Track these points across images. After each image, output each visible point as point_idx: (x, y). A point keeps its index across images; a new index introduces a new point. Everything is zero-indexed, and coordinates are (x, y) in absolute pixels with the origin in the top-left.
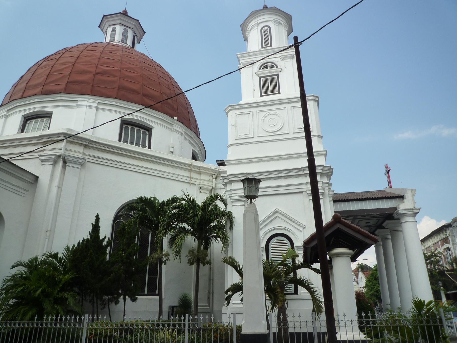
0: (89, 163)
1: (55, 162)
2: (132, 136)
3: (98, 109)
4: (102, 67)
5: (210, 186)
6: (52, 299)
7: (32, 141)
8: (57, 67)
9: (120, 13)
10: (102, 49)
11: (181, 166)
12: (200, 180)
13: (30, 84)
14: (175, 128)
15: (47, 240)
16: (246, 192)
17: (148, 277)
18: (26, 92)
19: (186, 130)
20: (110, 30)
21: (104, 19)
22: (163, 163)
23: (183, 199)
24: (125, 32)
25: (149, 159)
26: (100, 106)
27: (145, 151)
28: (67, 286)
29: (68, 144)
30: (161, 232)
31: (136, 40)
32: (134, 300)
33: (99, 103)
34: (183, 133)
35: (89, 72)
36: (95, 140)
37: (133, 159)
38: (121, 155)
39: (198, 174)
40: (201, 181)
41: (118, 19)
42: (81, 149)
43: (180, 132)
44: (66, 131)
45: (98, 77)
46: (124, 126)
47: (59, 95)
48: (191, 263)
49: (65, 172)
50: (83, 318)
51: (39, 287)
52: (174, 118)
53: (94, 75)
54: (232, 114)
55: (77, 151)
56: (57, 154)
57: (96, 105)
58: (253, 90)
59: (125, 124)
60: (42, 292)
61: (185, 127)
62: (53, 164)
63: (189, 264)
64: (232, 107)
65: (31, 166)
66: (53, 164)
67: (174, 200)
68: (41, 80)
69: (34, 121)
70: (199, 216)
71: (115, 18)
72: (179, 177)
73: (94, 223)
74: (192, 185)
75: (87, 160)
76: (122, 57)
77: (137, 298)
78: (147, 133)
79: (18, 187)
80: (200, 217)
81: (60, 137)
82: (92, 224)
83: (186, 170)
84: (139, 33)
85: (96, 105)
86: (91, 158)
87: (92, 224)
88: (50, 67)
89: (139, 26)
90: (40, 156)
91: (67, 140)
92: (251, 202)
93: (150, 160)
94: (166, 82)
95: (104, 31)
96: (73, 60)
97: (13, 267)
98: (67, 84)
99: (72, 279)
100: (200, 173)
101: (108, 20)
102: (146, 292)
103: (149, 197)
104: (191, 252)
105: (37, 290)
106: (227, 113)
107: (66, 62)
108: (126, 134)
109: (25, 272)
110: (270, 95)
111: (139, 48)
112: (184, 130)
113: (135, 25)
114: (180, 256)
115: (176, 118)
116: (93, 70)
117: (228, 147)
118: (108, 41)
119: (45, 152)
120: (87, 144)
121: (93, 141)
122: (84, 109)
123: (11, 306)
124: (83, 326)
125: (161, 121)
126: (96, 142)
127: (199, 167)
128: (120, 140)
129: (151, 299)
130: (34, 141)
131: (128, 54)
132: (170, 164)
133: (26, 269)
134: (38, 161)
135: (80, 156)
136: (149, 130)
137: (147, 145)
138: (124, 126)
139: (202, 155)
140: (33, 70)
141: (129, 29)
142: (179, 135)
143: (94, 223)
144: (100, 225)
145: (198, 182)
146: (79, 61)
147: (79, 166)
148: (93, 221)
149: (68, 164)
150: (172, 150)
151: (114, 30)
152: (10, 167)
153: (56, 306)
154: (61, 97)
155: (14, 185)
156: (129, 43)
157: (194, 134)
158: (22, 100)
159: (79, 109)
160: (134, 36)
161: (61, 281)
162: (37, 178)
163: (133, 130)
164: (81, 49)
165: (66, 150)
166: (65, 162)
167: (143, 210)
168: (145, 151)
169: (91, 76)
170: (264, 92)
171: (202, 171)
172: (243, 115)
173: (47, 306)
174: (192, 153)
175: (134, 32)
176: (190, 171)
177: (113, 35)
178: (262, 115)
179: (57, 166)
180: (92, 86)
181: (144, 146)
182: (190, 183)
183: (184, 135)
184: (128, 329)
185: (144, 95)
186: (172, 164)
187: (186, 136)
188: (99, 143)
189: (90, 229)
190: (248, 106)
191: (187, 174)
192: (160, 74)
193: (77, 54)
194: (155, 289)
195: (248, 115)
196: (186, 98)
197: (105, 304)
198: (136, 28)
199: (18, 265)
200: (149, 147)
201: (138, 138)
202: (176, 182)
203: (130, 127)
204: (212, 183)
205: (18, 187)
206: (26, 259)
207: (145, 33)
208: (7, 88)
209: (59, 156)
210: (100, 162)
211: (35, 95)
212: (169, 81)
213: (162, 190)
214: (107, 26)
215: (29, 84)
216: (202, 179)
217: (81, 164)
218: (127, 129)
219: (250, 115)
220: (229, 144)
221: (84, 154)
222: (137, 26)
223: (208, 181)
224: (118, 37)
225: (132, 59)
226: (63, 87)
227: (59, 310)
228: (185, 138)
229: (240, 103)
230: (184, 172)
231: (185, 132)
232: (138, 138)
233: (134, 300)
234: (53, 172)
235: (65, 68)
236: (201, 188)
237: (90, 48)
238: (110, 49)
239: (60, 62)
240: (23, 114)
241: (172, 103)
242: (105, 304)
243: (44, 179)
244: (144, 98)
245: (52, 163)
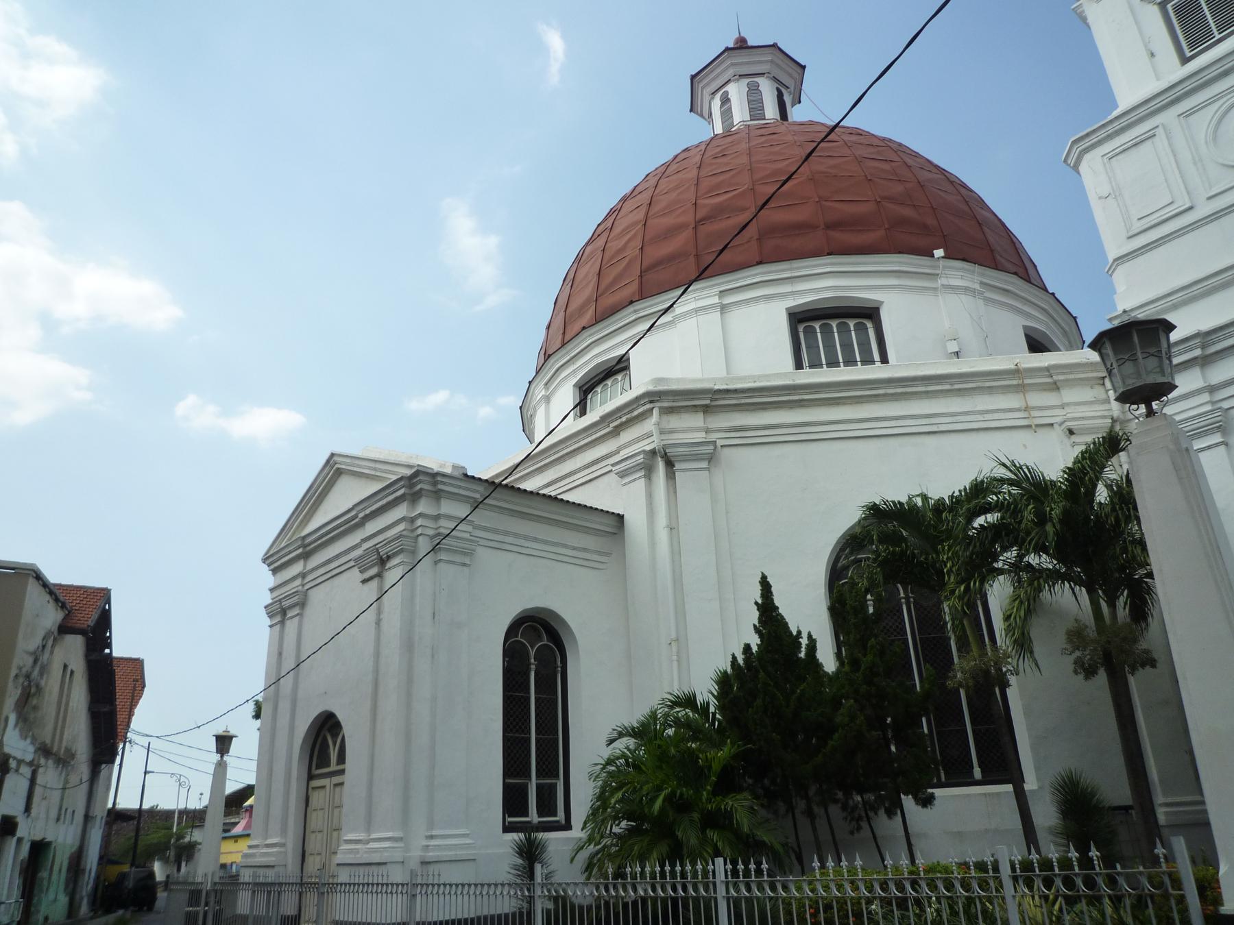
0: (726, 450)
1: (649, 470)
2: (830, 347)
3: (723, 308)
4: (707, 201)
5: (1104, 417)
6: (696, 816)
7: (590, 435)
8: (614, 246)
9: (727, 49)
10: (698, 158)
11: (987, 384)
12: (1063, 406)
13: (572, 308)
14: (944, 281)
15: (675, 664)
16: (1118, 379)
17: (974, 732)
18: (568, 328)
19: (982, 275)
20: (717, 103)
21: (696, 84)
22: (927, 392)
23: (1002, 481)
24: (754, 90)
25: (881, 392)
26: (727, 300)
27: (877, 372)
28: (727, 783)
29: (665, 417)
30: (953, 592)
31: (787, 99)
32: (927, 801)
33: (722, 293)
34: (977, 286)
35: (680, 227)
36: (725, 387)
37: (838, 404)
38: (801, 404)
39: (1051, 390)
40: (1068, 410)
41: (727, 68)
42: (697, 420)
43: (966, 289)
44: (651, 388)
45: (705, 229)
46: (801, 328)
47: (631, 309)
48: (1090, 672)
49: (675, 488)
50: (710, 867)
51: (659, 789)
52: (933, 256)
53: (695, 228)
54: (1093, 169)
55: (689, 429)
56: (648, 448)
57: (716, 300)
58: (1146, 58)
59: (801, 321)
60: (669, 799)
61: (977, 268)
62: (645, 476)
63: (1081, 677)
64: (1085, 144)
65: (603, 495)
66: (645, 476)
67: (979, 489)
68: (588, 291)
69: (599, 389)
70: (1056, 520)
71: (719, 70)
72: (988, 417)
73: (760, 601)
74: (1041, 431)
75: (720, 443)
76: (750, 154)
77: (932, 797)
78: (869, 325)
79: (584, 550)
80: (1060, 521)
81: (643, 405)
82: (756, 603)
83: (1006, 389)
84: (788, 73)
85: (716, 300)
86: (728, 435)
87: (756, 603)
88: (599, 253)
89: (781, 56)
90: (613, 465)
91: (660, 408)
92: (1150, 413)
93: (884, 395)
94: (886, 166)
95: (706, 114)
96: (640, 215)
97: (611, 742)
98: (641, 276)
99: (735, 757)
100: (1055, 387)
101: (705, 81)
102: (977, 773)
103: (904, 500)
104: (1076, 637)
105: (656, 797)
106: (1076, 167)
107: (627, 227)
108: (813, 347)
109: (629, 750)
110: (1219, 41)
111: (797, 114)
112: (977, 278)
113: (772, 61)
114: (1032, 652)
115: (939, 253)
116: (689, 218)
117: (1110, 272)
118: (719, 129)
119: (622, 453)
120: (708, 402)
121: (720, 391)
122: (692, 322)
123: (619, 836)
124: (715, 891)
125: (899, 277)
126: (728, 391)
127: (1047, 369)
128: (799, 365)
129: (998, 794)
130: (595, 433)
131: (763, 139)
132: (948, 387)
133: (631, 742)
134: (613, 477)
135: (700, 436)
136: (870, 313)
137: (876, 356)
138: (801, 328)
139: (1065, 333)
140: (571, 276)
141: (759, 80)
142: (965, 299)
143: (760, 601)
144: (777, 603)
145: (1057, 416)
146: (656, 208)
147: (704, 465)
148: (756, 594)
149: (677, 466)
150: (953, 347)
151: (726, 100)
152: (554, 507)
153: (709, 833)
154: (635, 311)
155: (574, 548)
156: (771, 112)
157: (1014, 279)
158: (563, 351)
159: (682, 326)
160: (778, 90)
161: (710, 767)
162: (620, 517)
163: (826, 330)
164: (653, 182)
165: (662, 433)
166: (669, 464)
167: (885, 539)
168: (877, 372)
169: (687, 234)
170: (1192, 45)
171: (1061, 377)
172: (1134, 151)
173: (688, 835)
174: (1027, 336)
175: (775, 79)
176: (1022, 389)
177: (727, 114)
178: (1203, 120)
179: (654, 477)
180: (697, 255)
181: (868, 360)
182: (1029, 426)
183: (981, 293)
184: (777, 898)
185: (831, 226)
186: (956, 387)
187: (988, 294)
188: (735, 391)
189: (754, 616)
190: (1142, 111)
191: (1013, 401)
192: (862, 152)
193: (645, 197)
194: (1001, 765)
195: (1149, 143)
196: (964, 186)
197: (860, 819)
198: (777, 65)
199: (621, 735)
200: (884, 360)
201: (847, 346)
202: (982, 435)
203: (817, 326)
204: (1106, 406)
205: (584, 550)
206: (634, 718)
207: (804, 67)
208: (538, 338)
209: (653, 452)
210: (753, 440)
211: (584, 328)
212: (896, 159)
213: (934, 469)
214: (707, 98)
215: (570, 310)
216: (1068, 404)
217: (710, 456)
218: (810, 332)
219: (1155, 139)
220: (1111, 261)
221: (708, 431)
222: (780, 62)
223: (1091, 403)
224: (740, 114)
225: (777, 148)
226: (634, 287)
227: (720, 845)
228: (986, 299)
229: (1115, 113)
230: (1001, 397)
231: (982, 283)
232: (847, 346)
233: (927, 801)
234: (650, 496)
235: (629, 240)
236: (1071, 432)
237: (674, 167)
238: (719, 149)
239: (617, 230)
240: (575, 381)
241: (939, 221)
242: (859, 819)
243: (636, 520)
244: (832, 233)
245: (642, 473)
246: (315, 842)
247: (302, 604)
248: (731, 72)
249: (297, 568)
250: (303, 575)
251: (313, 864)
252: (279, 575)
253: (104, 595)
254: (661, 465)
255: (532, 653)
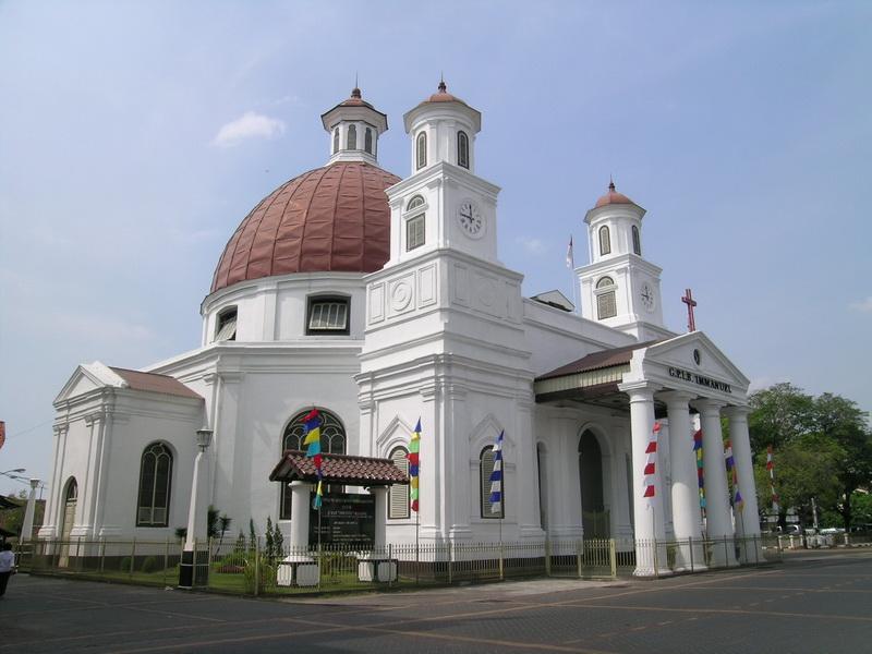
3: (278, 292)
8: (243, 241)
24: (352, 131)
26: (282, 287)
57: (275, 287)
122: (263, 296)
137: (454, 307)
141: (356, 124)
166: (223, 379)
169: (271, 246)
185: (334, 253)
226: (243, 271)
246: (67, 528)
247: (67, 428)
248: (340, 119)
249: (65, 412)
250: (67, 416)
251: (66, 534)
252: (344, 292)
253: (523, 276)
254: (219, 379)
255: (157, 458)
